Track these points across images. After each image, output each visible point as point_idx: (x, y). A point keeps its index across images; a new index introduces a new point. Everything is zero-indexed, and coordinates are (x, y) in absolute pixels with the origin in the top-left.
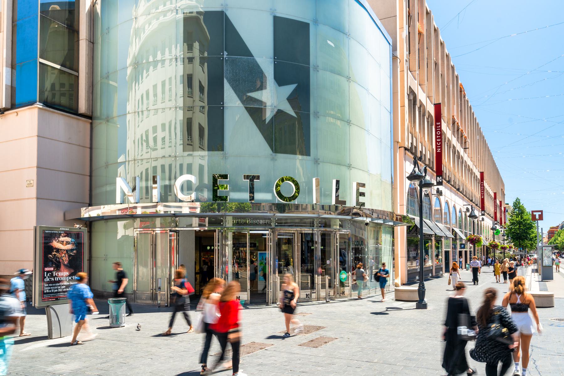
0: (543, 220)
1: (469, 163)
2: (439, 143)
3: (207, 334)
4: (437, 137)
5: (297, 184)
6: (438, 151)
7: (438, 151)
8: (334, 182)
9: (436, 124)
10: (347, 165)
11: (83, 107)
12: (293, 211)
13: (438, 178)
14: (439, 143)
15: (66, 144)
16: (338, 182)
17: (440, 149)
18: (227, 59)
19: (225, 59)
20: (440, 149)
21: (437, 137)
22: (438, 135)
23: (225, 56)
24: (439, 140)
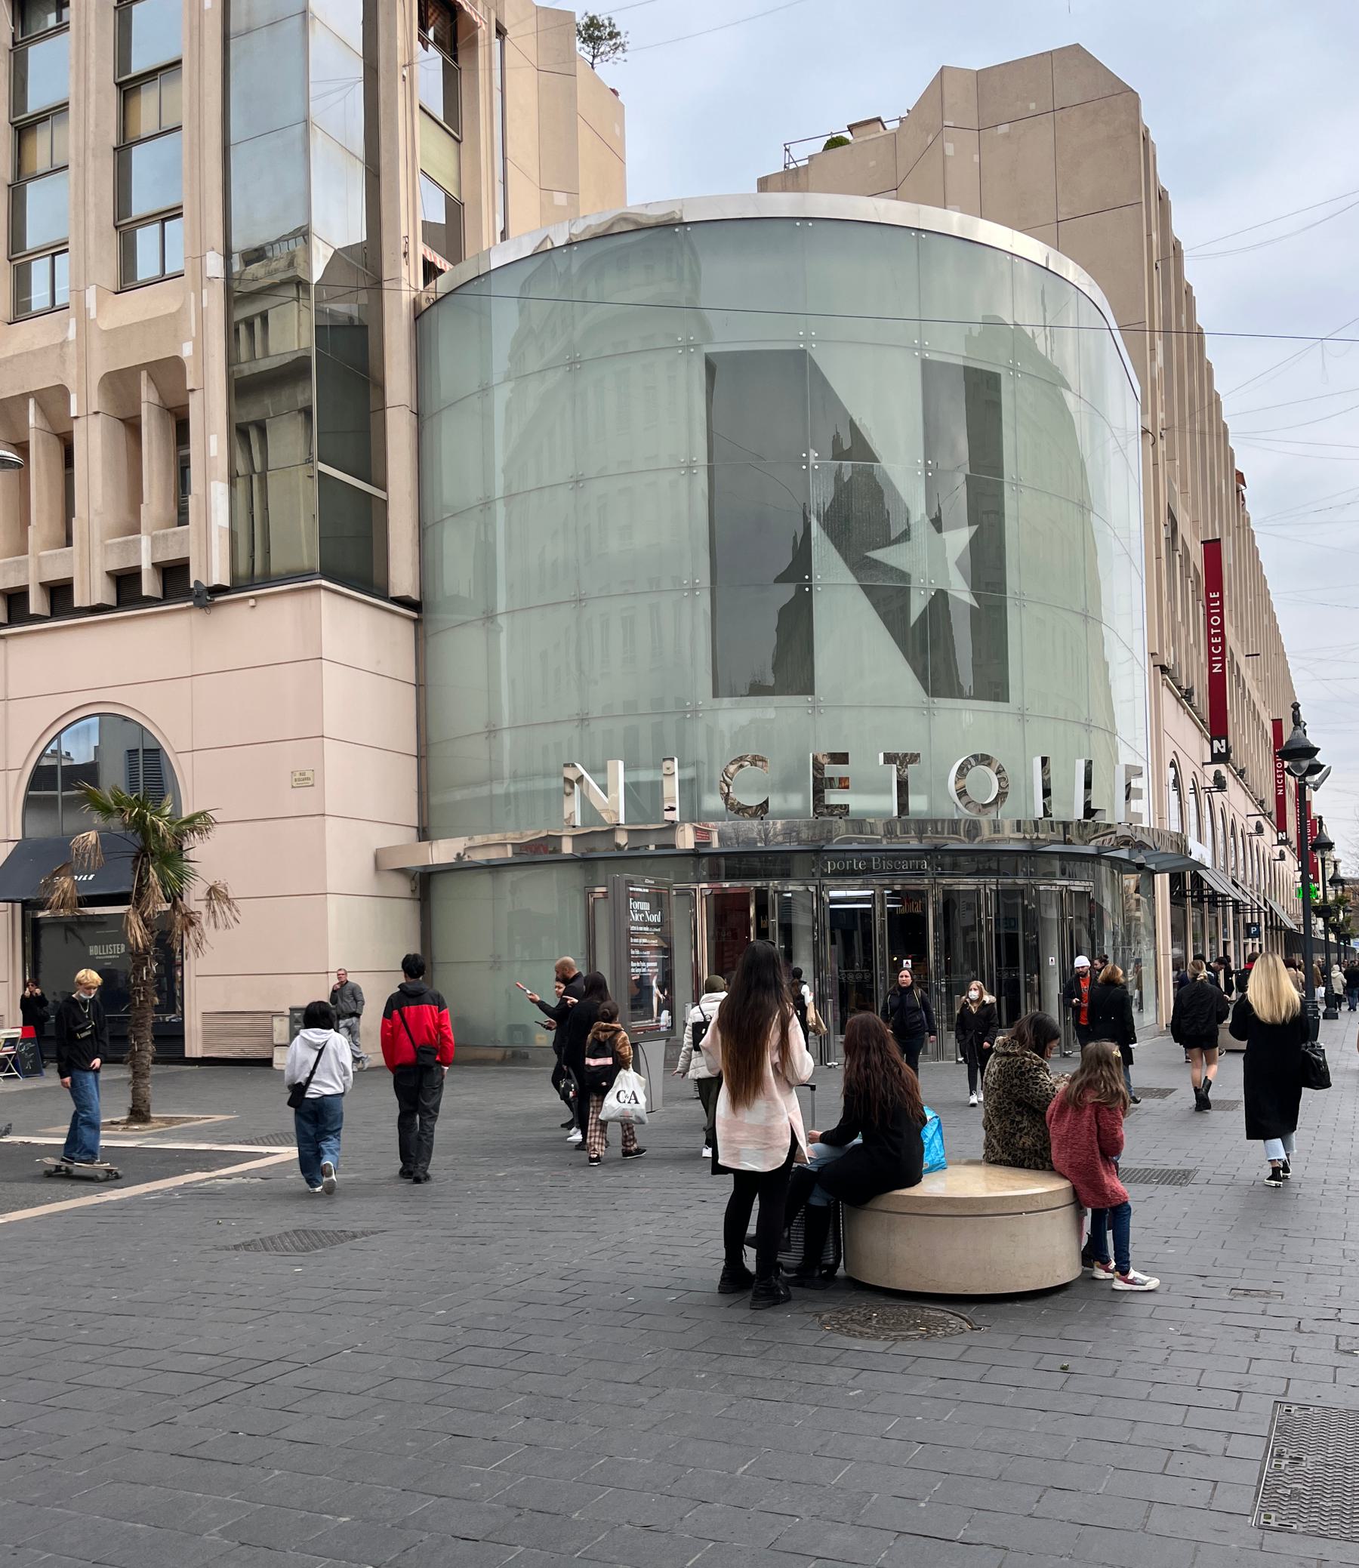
0: (1008, 701)
1: (1256, 696)
2: (1216, 649)
3: (754, 1237)
4: (1213, 631)
5: (1002, 796)
6: (1215, 671)
7: (1215, 671)
8: (1038, 762)
9: (1207, 595)
10: (1084, 722)
11: (403, 579)
12: (946, 835)
13: (1216, 743)
14: (1216, 649)
15: (409, 828)
16: (1044, 760)
17: (1220, 665)
18: (816, 467)
19: (813, 467)
20: (1220, 665)
21: (1213, 631)
22: (1215, 628)
23: (812, 461)
24: (1216, 641)
